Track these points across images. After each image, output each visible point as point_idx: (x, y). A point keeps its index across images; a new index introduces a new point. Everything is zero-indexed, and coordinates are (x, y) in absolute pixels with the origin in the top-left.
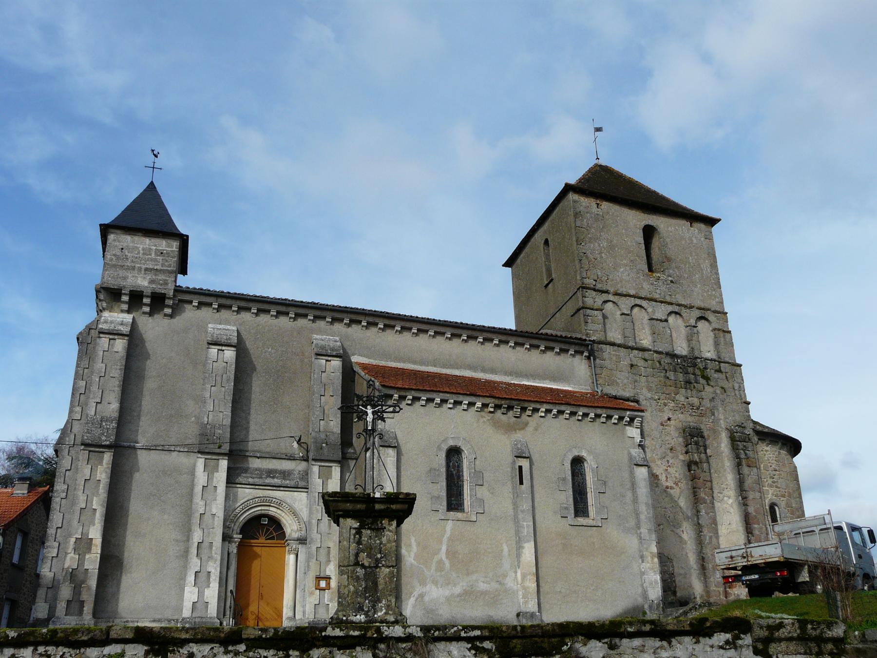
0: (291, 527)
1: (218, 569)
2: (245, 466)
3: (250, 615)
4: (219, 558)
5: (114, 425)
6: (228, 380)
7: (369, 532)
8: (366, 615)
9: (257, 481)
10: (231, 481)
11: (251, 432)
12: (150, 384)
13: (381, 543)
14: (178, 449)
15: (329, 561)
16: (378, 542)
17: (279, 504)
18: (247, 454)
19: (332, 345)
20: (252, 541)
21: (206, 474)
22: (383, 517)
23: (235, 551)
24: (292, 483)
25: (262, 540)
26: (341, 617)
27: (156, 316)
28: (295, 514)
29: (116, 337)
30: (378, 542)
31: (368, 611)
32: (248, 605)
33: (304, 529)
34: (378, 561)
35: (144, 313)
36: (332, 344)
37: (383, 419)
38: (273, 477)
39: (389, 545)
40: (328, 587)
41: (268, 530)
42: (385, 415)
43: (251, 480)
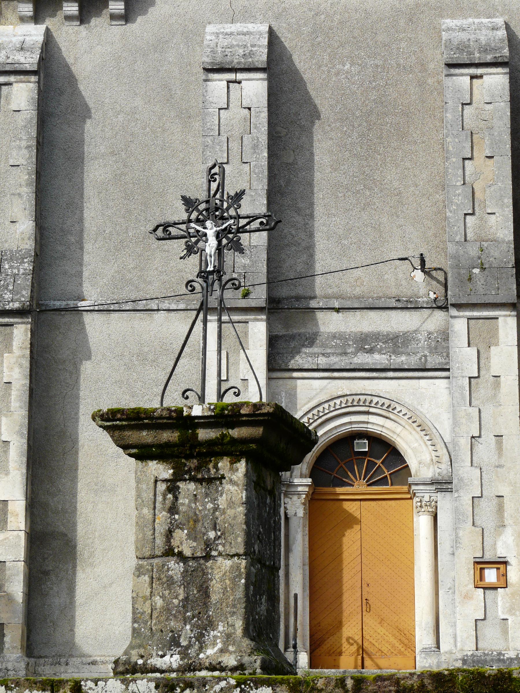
0: (419, 457)
2: (308, 330)
3: (345, 645)
5: (28, 266)
6: (255, 147)
7: (192, 486)
8: (184, 654)
9: (335, 361)
11: (318, 256)
12: (96, 171)
13: (216, 509)
14: (166, 305)
16: (210, 506)
17: (389, 408)
18: (313, 304)
19: (483, 40)
20: (339, 490)
22: (220, 455)
23: (301, 512)
24: (413, 361)
25: (360, 487)
26: (134, 659)
27: (94, 21)
29: (12, 79)
30: (210, 506)
31: (188, 647)
32: (339, 625)
33: (446, 458)
34: (209, 545)
35: (68, 18)
36: (484, 36)
37: (238, 247)
38: (371, 351)
39: (230, 512)
41: (371, 464)
42: (244, 237)
43: (322, 362)
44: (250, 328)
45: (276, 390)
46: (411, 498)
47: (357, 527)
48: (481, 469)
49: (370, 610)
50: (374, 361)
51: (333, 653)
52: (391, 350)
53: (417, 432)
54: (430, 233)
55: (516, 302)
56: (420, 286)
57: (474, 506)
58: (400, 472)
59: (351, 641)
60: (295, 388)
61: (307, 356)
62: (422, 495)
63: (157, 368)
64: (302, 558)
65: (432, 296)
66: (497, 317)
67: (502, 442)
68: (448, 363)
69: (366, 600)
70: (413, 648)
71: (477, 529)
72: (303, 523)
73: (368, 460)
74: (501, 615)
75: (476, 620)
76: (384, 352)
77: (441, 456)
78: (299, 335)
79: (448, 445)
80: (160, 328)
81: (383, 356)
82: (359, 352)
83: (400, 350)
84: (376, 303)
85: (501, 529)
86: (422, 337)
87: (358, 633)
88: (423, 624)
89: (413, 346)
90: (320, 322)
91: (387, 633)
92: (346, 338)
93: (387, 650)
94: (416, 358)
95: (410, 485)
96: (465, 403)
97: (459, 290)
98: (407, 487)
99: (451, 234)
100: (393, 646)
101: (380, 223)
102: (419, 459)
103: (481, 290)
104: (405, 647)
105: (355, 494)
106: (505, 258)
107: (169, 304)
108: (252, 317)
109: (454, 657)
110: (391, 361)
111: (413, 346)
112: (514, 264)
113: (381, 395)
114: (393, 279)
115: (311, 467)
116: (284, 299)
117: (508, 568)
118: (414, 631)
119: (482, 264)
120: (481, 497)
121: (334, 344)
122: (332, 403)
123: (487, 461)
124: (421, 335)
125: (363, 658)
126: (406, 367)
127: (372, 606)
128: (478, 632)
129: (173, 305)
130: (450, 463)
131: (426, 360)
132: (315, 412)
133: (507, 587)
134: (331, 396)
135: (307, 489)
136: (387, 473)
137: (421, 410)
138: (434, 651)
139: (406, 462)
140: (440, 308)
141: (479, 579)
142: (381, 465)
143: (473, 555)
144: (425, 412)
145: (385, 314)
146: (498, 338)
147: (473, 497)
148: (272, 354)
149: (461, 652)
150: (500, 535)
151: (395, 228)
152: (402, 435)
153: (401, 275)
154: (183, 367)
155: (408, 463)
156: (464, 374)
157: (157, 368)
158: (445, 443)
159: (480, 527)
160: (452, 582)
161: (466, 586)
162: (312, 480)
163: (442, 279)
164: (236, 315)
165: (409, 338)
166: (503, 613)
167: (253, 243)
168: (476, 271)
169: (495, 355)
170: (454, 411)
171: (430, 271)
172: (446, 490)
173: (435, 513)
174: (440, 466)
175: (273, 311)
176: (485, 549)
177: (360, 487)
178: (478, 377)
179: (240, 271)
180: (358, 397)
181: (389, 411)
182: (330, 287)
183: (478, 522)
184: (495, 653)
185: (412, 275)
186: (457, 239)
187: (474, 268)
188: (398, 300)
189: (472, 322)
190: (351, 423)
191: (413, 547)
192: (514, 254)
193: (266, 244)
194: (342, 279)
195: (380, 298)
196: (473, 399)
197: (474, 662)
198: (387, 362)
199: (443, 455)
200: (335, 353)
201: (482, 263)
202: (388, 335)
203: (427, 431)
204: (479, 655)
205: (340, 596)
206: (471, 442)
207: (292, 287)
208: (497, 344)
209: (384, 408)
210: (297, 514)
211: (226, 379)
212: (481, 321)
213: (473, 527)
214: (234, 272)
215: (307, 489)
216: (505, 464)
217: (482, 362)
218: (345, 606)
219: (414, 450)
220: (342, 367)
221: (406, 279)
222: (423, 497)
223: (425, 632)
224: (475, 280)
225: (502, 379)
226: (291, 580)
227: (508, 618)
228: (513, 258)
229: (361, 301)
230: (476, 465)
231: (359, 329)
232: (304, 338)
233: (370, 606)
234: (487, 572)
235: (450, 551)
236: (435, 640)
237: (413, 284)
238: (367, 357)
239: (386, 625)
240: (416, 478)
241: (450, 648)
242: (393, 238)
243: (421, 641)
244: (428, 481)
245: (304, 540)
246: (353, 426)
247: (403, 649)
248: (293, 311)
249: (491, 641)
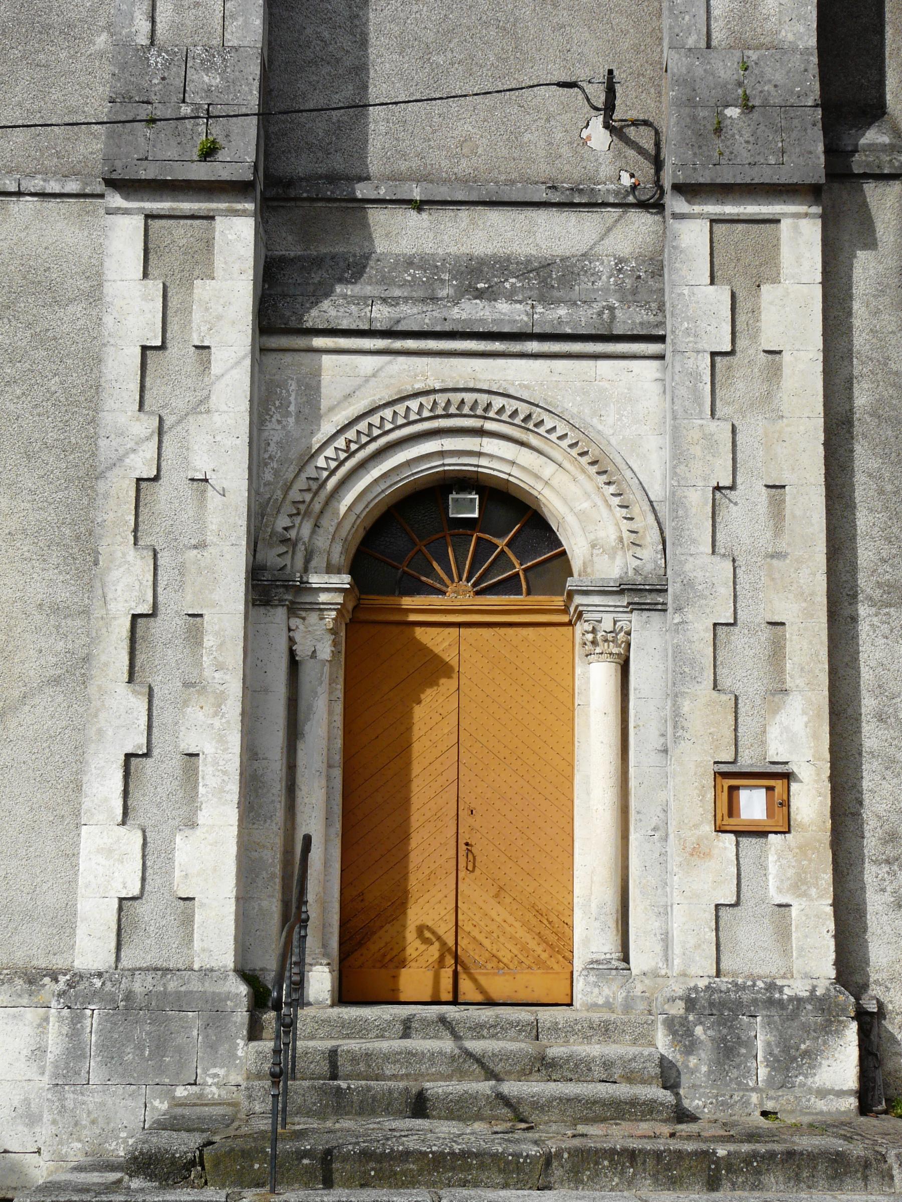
0: (590, 531)
1: (235, 740)
3: (413, 946)
4: (235, 687)
9: (413, 315)
10: (280, 313)
14: (36, 184)
15: (779, 691)
17: (526, 422)
18: (362, 191)
20: (407, 602)
21: (155, 287)
23: (325, 651)
24: (584, 318)
25: (459, 596)
28: (601, 466)
33: (653, 536)
38: (488, 295)
40: (781, 820)
41: (484, 548)
43: (381, 315)
44: (217, 229)
45: (277, 377)
46: (570, 624)
47: (447, 685)
48: (734, 561)
49: (474, 867)
50: (497, 316)
51: (391, 960)
52: (535, 293)
53: (589, 477)
54: (626, 44)
55: (823, 181)
56: (601, 160)
57: (718, 644)
58: (548, 565)
59: (427, 934)
60: (317, 373)
61: (348, 303)
62: (597, 616)
63: (14, 323)
64: (325, 752)
65: (626, 180)
66: (777, 217)
67: (784, 501)
68: (662, 324)
69: (467, 844)
70: (567, 954)
71: (724, 698)
72: (331, 674)
73: (478, 538)
74: (775, 896)
75: (717, 907)
76: (520, 297)
77: (641, 531)
78: (333, 258)
79: (657, 508)
80: (23, 235)
81: (518, 306)
82: (463, 296)
83: (556, 293)
84: (503, 191)
85: (777, 698)
86: (603, 267)
88: (594, 905)
89: (583, 286)
90: (378, 234)
92: (437, 267)
93: (509, 956)
94: (590, 312)
95: (571, 595)
96: (701, 412)
97: (695, 154)
98: (561, 598)
99: (677, 30)
100: (524, 948)
101: (516, 20)
102: (592, 537)
103: (744, 154)
104: (549, 950)
105: (443, 611)
106: (798, 86)
107: (44, 181)
108: (223, 206)
109: (667, 993)
110: (535, 316)
111: (583, 285)
112: (817, 97)
113: (512, 392)
114: (541, 143)
115: (353, 551)
116: (301, 179)
117: (792, 788)
118: (571, 916)
119: (746, 98)
120: (734, 624)
121: (409, 278)
122: (400, 408)
123: (748, 542)
124: (602, 263)
125: (456, 974)
126: (569, 331)
127: (478, 859)
128: (721, 934)
129: (52, 183)
130: (661, 547)
131: (613, 317)
132: (362, 426)
133: (789, 832)
134: (400, 391)
135: (339, 598)
136: (518, 568)
137: (600, 427)
138: (616, 969)
139: (560, 544)
140: (642, 205)
141: (725, 811)
142: (506, 549)
143: (713, 757)
144: (608, 431)
145: (523, 216)
146: (777, 266)
147: (715, 625)
148: (271, 295)
149: (681, 979)
150: (775, 711)
151: (549, 31)
152: (554, 482)
153: (559, 135)
154: (73, 322)
155: (566, 546)
156: (700, 346)
157: (14, 323)
158: (651, 502)
159: (731, 692)
160: (662, 815)
161: (696, 826)
162: (353, 577)
163: (648, 144)
164: (187, 201)
165: (576, 270)
166: (780, 890)
167: (229, 40)
168: (733, 112)
169: (771, 303)
170: (675, 429)
171: (622, 127)
172: (652, 608)
173: (624, 657)
174: (639, 552)
175: (275, 204)
176: (740, 743)
177: (459, 596)
178: (732, 353)
179: (198, 101)
180: (459, 396)
181: (528, 429)
182: (404, 155)
183: (726, 682)
184: (760, 984)
185: (584, 135)
186: (691, 42)
187: (727, 106)
188: (554, 188)
189: (720, 229)
190: (442, 454)
191: (573, 730)
192: (817, 78)
193: (259, 45)
194: (429, 140)
195: (513, 182)
196: (718, 404)
197: (712, 1004)
198: (526, 319)
199: (646, 528)
200: (411, 298)
201: (745, 94)
202: (529, 261)
203: (612, 475)
204: (724, 988)
205: (405, 837)
206: (714, 500)
207: (320, 154)
208: (775, 280)
209: (517, 421)
210: (318, 653)
211: (159, 344)
212: (740, 227)
213: (715, 693)
214: (184, 101)
215: (339, 598)
216: (789, 551)
217: (741, 319)
218: (414, 859)
219: (581, 516)
220: (426, 328)
221: (571, 143)
222: (600, 622)
223: (597, 924)
224: (730, 132)
225: (786, 357)
226: (299, 801)
227: (790, 902)
228: (817, 86)
229: (472, 188)
230: (722, 551)
231: (465, 250)
232: (342, 264)
233: (474, 858)
234: (744, 796)
235: (658, 743)
236: (619, 942)
237: (586, 156)
238: (481, 306)
239: (508, 900)
240: (584, 578)
241: (653, 964)
242: (544, 52)
243: (586, 941)
244: (612, 586)
245: (330, 713)
246: (447, 461)
247: (544, 956)
248: (320, 204)
249: (750, 955)
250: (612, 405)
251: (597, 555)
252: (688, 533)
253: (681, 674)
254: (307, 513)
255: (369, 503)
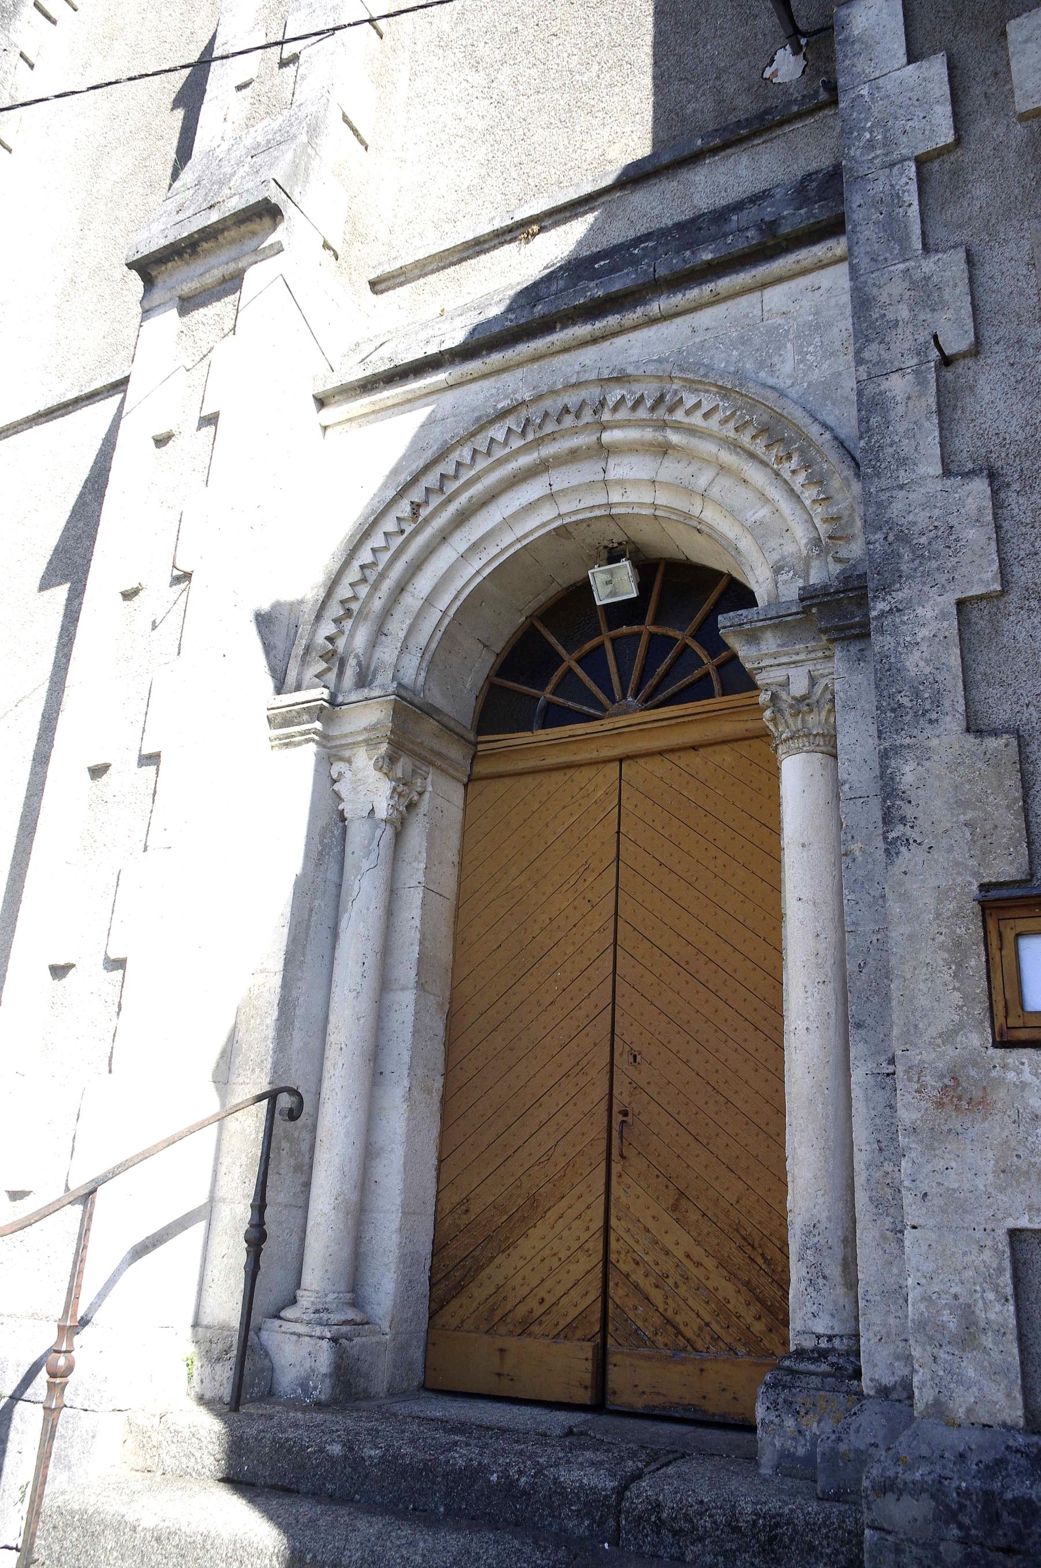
71: (993, 743)
87: (590, 1245)
91: (698, 1253)
93: (695, 1323)
96: (904, 249)
100: (721, 1309)
102: (775, 556)
143: (976, 874)
250: (789, 345)
251: (785, 582)
252: (891, 450)
253: (893, 710)
254: (362, 615)
255: (459, 592)
